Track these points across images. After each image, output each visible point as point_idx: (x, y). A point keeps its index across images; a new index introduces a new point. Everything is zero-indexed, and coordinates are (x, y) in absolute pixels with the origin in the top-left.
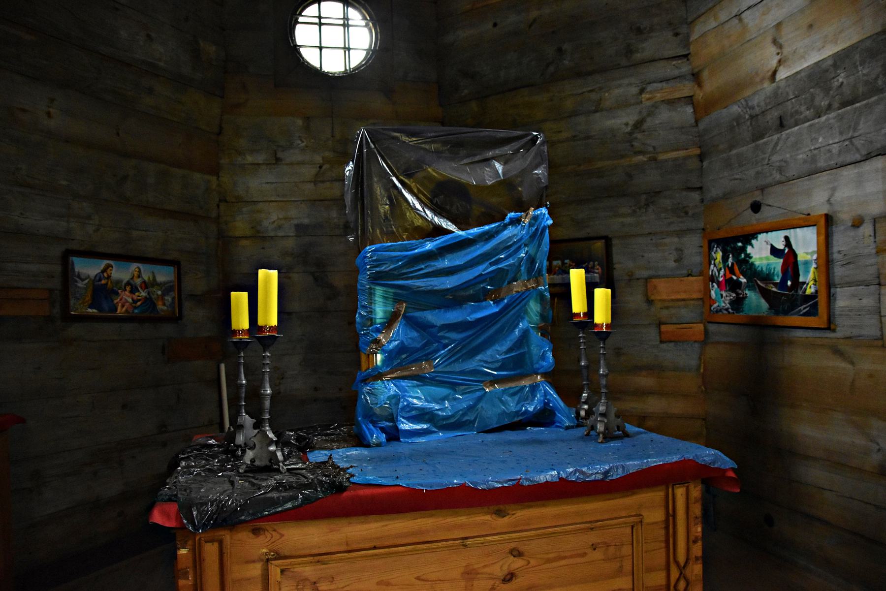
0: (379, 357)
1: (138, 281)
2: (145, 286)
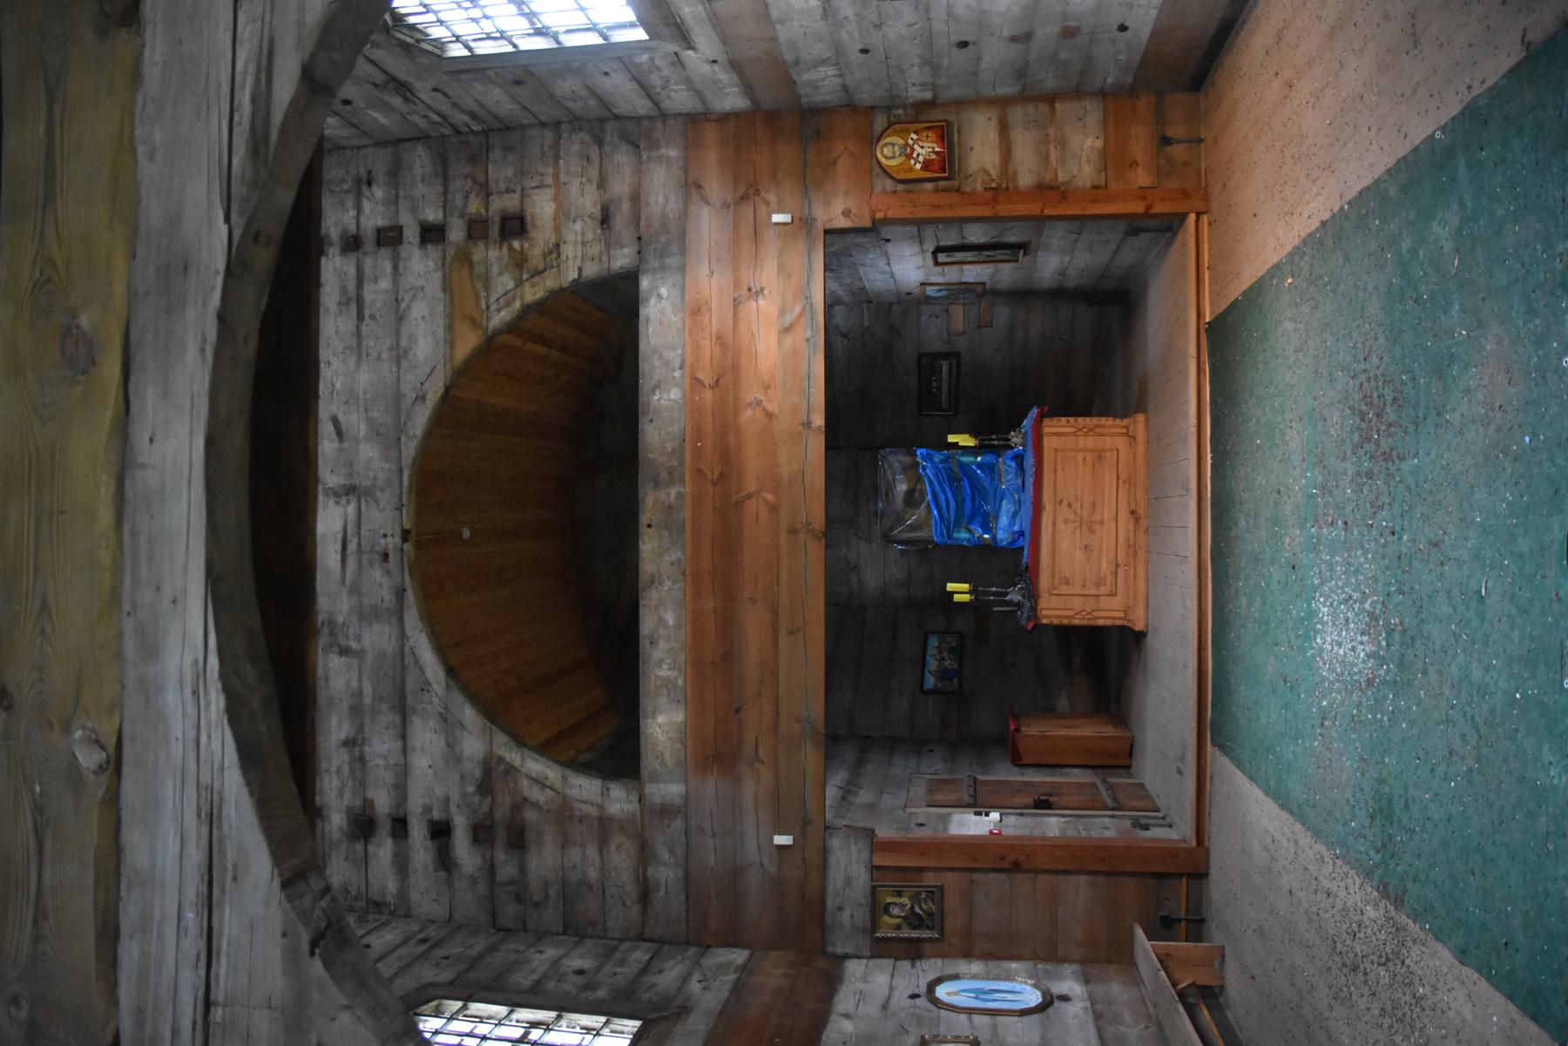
0: (986, 536)
1: (938, 656)
2: (940, 653)
